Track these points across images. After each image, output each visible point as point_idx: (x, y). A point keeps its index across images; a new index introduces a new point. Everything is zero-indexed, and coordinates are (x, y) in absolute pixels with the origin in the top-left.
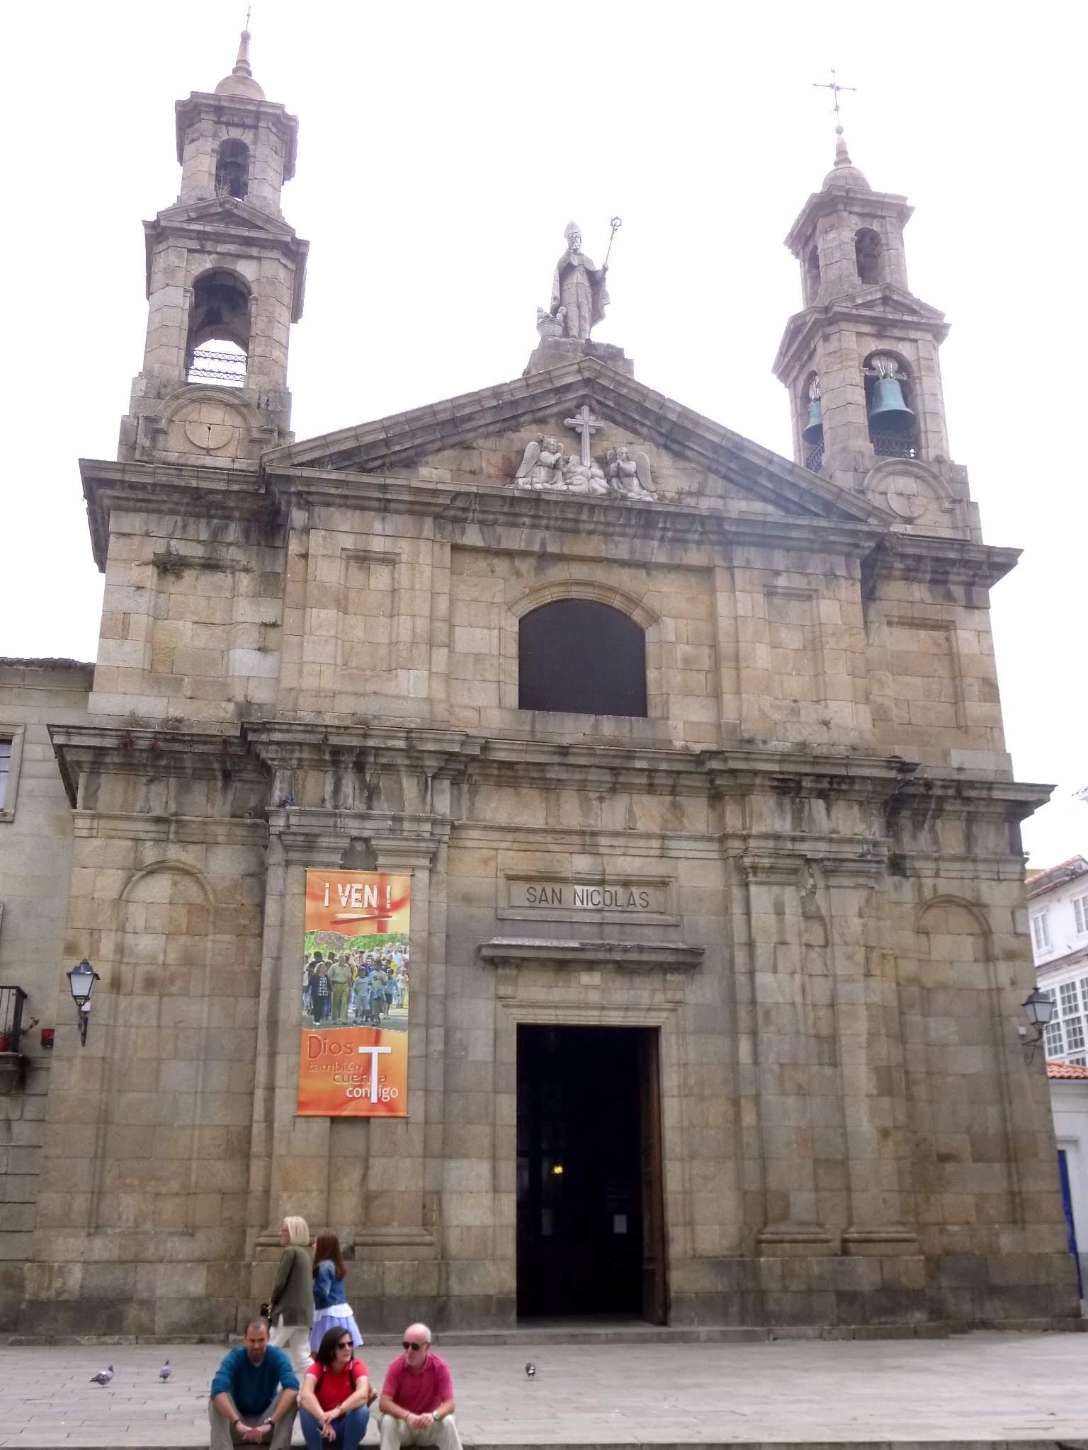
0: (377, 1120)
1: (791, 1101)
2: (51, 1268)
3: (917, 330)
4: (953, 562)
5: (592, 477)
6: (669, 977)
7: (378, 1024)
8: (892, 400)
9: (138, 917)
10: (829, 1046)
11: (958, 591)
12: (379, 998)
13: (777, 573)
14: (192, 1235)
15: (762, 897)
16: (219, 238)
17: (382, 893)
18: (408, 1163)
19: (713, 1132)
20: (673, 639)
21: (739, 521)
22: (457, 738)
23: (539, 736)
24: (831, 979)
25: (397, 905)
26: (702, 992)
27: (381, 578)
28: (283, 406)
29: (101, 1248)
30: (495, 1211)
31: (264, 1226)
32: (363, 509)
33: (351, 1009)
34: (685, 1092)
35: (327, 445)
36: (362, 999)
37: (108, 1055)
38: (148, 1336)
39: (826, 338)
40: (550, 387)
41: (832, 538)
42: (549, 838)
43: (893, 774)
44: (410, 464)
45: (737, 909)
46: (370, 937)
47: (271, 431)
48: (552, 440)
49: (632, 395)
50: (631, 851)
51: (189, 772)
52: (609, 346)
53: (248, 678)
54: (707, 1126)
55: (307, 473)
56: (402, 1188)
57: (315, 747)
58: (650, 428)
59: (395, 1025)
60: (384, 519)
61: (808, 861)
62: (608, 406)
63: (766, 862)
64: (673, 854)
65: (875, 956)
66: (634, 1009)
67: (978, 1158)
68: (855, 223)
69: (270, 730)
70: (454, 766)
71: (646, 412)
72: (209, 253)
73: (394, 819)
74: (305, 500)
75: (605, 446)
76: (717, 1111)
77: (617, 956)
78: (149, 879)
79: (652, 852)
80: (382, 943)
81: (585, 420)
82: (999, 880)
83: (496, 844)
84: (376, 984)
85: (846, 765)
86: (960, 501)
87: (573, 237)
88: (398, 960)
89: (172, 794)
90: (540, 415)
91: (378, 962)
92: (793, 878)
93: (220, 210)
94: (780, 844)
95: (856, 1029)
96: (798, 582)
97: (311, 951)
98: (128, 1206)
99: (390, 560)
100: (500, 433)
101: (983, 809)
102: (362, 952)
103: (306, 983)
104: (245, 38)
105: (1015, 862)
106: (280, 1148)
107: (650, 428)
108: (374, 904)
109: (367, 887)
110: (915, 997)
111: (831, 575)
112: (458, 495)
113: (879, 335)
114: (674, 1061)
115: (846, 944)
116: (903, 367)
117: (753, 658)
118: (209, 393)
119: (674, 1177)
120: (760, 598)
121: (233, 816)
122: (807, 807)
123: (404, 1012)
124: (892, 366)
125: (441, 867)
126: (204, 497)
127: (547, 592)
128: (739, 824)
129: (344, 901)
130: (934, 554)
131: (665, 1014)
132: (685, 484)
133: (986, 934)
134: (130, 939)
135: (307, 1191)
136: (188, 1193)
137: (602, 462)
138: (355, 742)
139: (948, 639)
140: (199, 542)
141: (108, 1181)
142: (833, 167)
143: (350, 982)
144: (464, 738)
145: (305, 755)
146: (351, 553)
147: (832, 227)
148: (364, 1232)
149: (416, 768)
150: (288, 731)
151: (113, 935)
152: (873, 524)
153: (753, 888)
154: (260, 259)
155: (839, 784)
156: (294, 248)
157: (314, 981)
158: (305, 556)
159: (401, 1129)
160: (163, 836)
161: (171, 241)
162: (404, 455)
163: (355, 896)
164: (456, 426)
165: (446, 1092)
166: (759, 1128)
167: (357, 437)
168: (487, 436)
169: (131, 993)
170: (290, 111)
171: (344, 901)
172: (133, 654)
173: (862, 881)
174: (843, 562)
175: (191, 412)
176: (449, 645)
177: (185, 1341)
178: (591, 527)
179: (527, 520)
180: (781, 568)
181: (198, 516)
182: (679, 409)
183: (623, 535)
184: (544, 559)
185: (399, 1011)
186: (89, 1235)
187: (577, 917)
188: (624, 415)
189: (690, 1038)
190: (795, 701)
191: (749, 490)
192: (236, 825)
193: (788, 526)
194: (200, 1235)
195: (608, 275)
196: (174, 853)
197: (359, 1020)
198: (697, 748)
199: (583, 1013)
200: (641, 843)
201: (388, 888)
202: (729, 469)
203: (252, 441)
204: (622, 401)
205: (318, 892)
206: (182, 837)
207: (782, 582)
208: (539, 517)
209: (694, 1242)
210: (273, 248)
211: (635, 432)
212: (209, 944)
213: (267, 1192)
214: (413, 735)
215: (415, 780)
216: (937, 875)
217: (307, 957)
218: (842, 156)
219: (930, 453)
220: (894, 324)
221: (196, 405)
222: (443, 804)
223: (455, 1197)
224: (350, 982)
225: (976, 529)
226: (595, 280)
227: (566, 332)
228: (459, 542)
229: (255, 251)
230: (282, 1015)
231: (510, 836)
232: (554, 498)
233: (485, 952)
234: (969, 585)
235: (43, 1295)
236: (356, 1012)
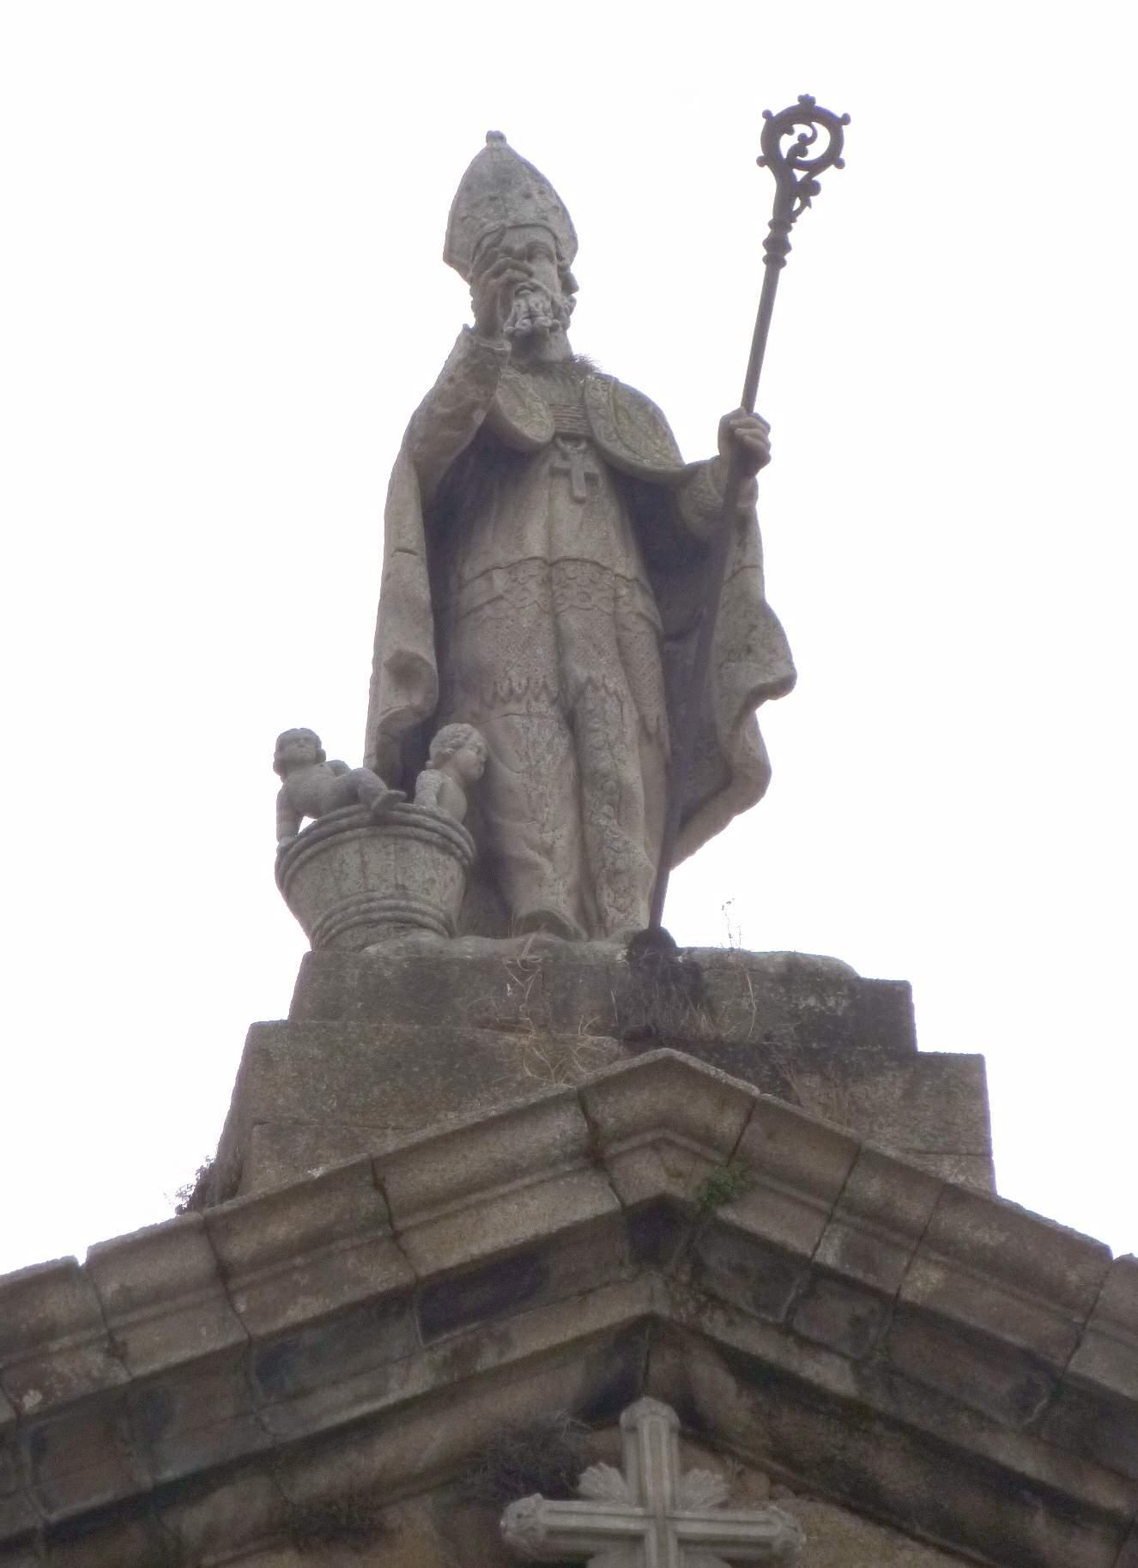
40: (381, 1277)
49: (982, 1306)
62: (810, 1397)
87: (508, 237)
188: (930, 1449)
195: (775, 498)
226: (687, 532)
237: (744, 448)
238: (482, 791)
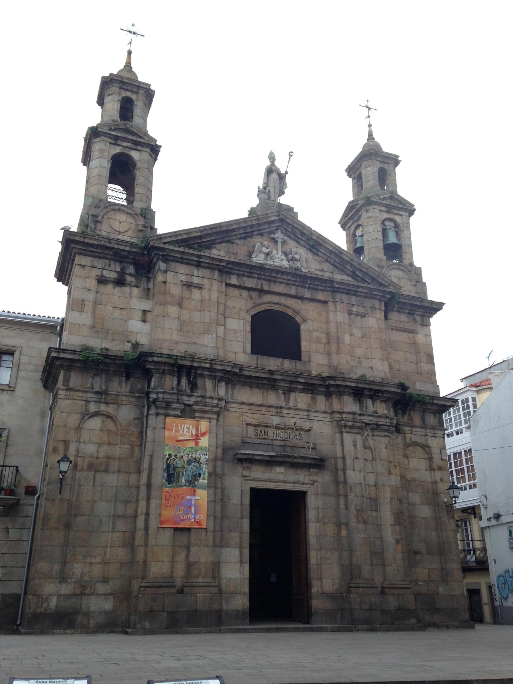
0: (193, 530)
1: (361, 526)
2: (42, 598)
3: (403, 211)
4: (417, 306)
5: (282, 260)
6: (311, 470)
7: (195, 486)
8: (392, 239)
9: (85, 436)
10: (374, 502)
11: (418, 318)
12: (195, 475)
13: (353, 305)
14: (107, 582)
15: (348, 438)
16: (124, 139)
17: (197, 429)
18: (206, 549)
19: (329, 538)
20: (312, 329)
21: (339, 283)
22: (231, 364)
23: (259, 366)
24: (375, 474)
25: (203, 434)
26: (324, 478)
27: (196, 294)
28: (152, 217)
29: (66, 589)
30: (242, 572)
31: (143, 578)
32: (190, 264)
33: (184, 479)
34: (318, 520)
35: (176, 236)
36: (188, 475)
37: (71, 499)
38: (87, 630)
39: (367, 211)
40: (266, 220)
41: (375, 293)
42: (264, 409)
43: (399, 391)
44: (209, 246)
45: (338, 442)
46: (192, 448)
47: (147, 227)
48: (267, 243)
49: (299, 227)
50: (296, 416)
51: (111, 372)
52: (288, 206)
53: (137, 333)
54: (326, 535)
55: (168, 247)
56: (204, 561)
57: (172, 365)
58: (304, 241)
59: (202, 487)
60: (198, 270)
61: (367, 424)
62: (288, 231)
63: (350, 424)
64: (312, 418)
65: (392, 465)
66: (297, 483)
67: (429, 553)
68: (378, 165)
69: (153, 356)
70: (228, 376)
71: (302, 233)
72: (119, 145)
73: (202, 397)
74: (166, 259)
75: (287, 248)
76: (330, 529)
77: (290, 460)
78: (91, 419)
79: (304, 417)
80: (197, 451)
81: (279, 235)
82: (435, 437)
83: (246, 412)
84: (194, 468)
85: (382, 386)
86: (419, 282)
87: (272, 158)
88: (203, 459)
89: (103, 382)
90: (261, 232)
91: (195, 459)
92: (360, 431)
93: (124, 127)
94: (356, 416)
95: (386, 495)
96: (361, 310)
97: (167, 453)
98: (77, 569)
99: (199, 287)
100: (245, 238)
101: (429, 407)
102: (188, 454)
103: (165, 467)
104: (130, 53)
105: (441, 430)
106: (151, 542)
107: (304, 241)
108: (194, 434)
109: (191, 426)
110: (407, 484)
111: (373, 308)
112: (229, 262)
113: (388, 212)
114: (313, 507)
115: (381, 460)
116: (396, 226)
117: (339, 338)
118: (120, 207)
119: (314, 557)
120: (346, 315)
121: (130, 392)
122: (365, 401)
123: (206, 481)
124: (392, 225)
125: (221, 419)
126: (111, 250)
127: (262, 306)
128: (339, 408)
129: (181, 432)
130: (411, 302)
131: (309, 486)
132: (318, 267)
133: (430, 459)
134: (82, 446)
135: (163, 562)
136: (104, 562)
137: (285, 254)
138: (188, 363)
139: (414, 337)
140: (115, 272)
141: (69, 557)
142: (367, 141)
143: (183, 467)
144: (233, 365)
145: (166, 368)
146: (184, 283)
147: (370, 166)
148: (187, 581)
149: (213, 377)
150: (161, 357)
151: (75, 444)
152: (391, 289)
153: (345, 434)
154: (140, 151)
155: (378, 393)
156: (155, 148)
157: (168, 466)
158: (165, 282)
159: (204, 533)
160: (99, 400)
161: (102, 138)
162: (206, 243)
163: (186, 430)
164: (228, 233)
165: (222, 517)
166: (348, 537)
167: (188, 233)
168: (240, 239)
169: (82, 470)
170: (152, 88)
171: (181, 432)
172: (85, 319)
173: (387, 434)
174: (378, 303)
175: (112, 215)
176: (224, 325)
177: (103, 632)
178: (281, 280)
179: (256, 276)
180: (355, 303)
181: (116, 261)
182: (317, 235)
183: (294, 285)
184: (262, 292)
185: (203, 481)
186: (60, 582)
187: (275, 443)
188: (294, 235)
189: (320, 497)
190: (359, 358)
191: (342, 270)
192: (131, 396)
193: (358, 287)
194: (111, 583)
195: (287, 176)
196: (103, 408)
197: (187, 484)
198: (324, 375)
199: (276, 484)
200: (300, 413)
201: (200, 427)
202: (335, 261)
203: (139, 231)
204: (294, 229)
205: (171, 428)
206: (107, 401)
207: (354, 309)
208: (262, 275)
209: (322, 586)
210: (147, 147)
211: (298, 243)
212: (118, 449)
213: (145, 562)
214: (213, 362)
215: (211, 381)
216: (411, 433)
217: (165, 456)
218: (371, 136)
219: (406, 262)
220: (395, 208)
221: (113, 212)
222: (222, 391)
223: (224, 565)
224: (183, 467)
225: (425, 293)
226: (282, 177)
227: (269, 198)
228: (228, 282)
229: (139, 148)
230: (154, 481)
231: (248, 407)
232: (268, 267)
233: (239, 456)
234: (423, 316)
235: (38, 611)
236: (186, 480)
237: (286, 173)
238: (269, 191)
